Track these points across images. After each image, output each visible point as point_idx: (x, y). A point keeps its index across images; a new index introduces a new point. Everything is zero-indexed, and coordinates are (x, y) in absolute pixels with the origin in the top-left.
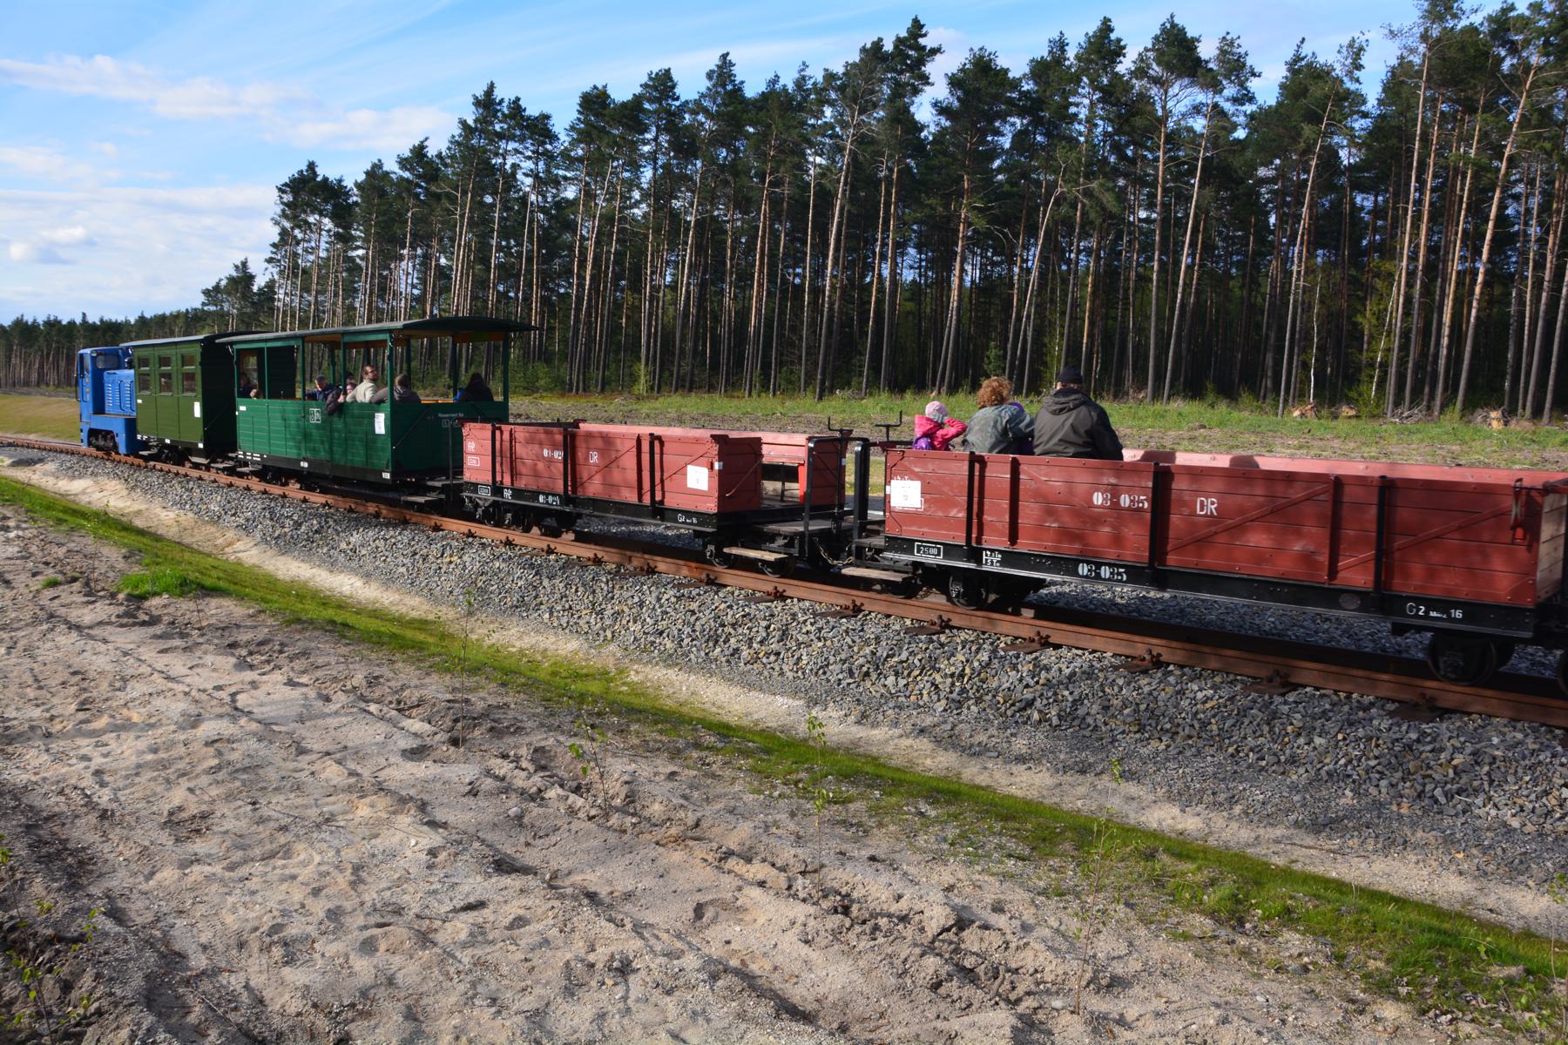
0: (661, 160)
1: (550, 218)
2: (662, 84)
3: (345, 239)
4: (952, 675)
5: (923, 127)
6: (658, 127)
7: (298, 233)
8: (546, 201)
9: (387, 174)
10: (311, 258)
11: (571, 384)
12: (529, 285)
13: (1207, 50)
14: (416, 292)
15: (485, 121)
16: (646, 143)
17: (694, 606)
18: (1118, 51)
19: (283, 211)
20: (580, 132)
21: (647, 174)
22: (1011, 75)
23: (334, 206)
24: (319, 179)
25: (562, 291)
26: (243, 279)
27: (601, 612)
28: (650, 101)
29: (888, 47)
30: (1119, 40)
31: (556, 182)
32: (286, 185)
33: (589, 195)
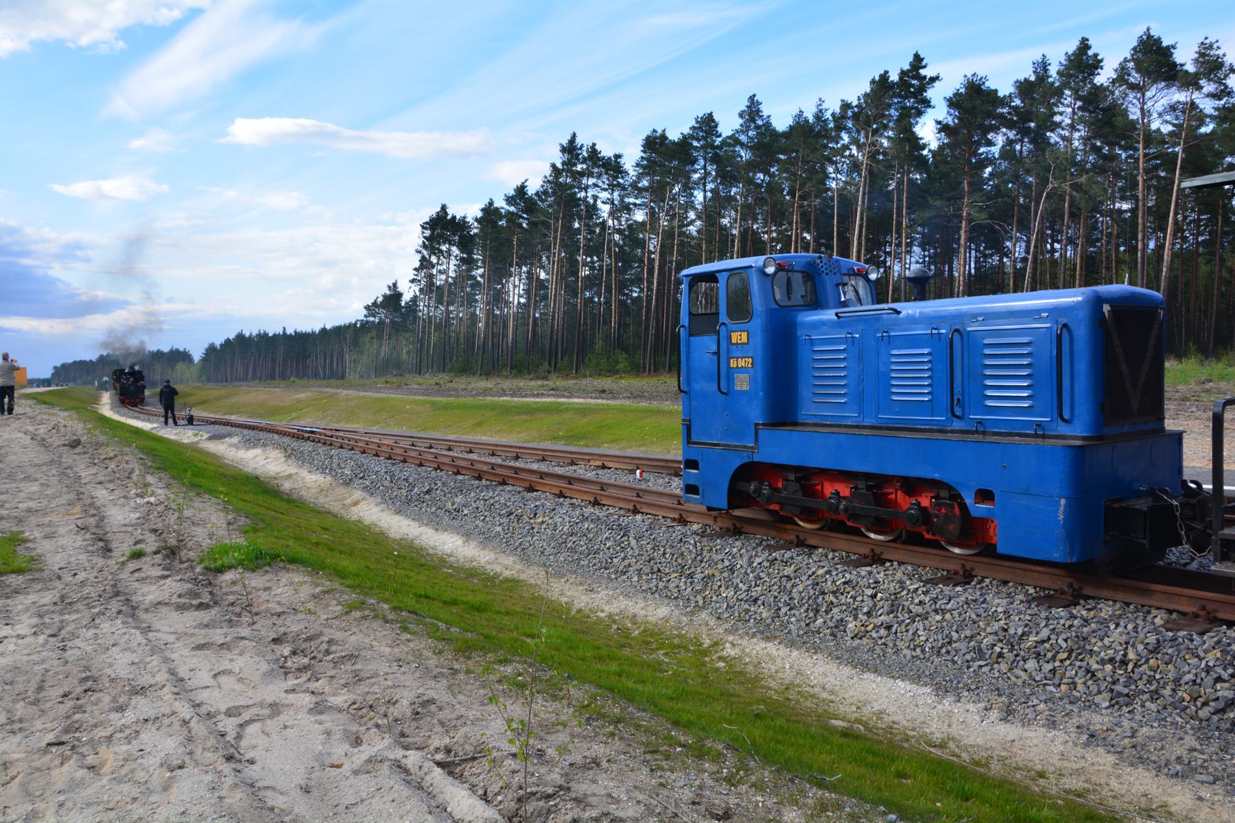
0: (710, 186)
1: (624, 237)
2: (707, 124)
3: (468, 262)
4: (1112, 660)
5: (924, 147)
6: (705, 159)
7: (434, 259)
8: (621, 225)
9: (497, 209)
10: (443, 277)
11: (645, 367)
12: (609, 290)
13: (1185, 57)
14: (522, 300)
15: (569, 164)
16: (696, 171)
17: (789, 571)
18: (1096, 64)
19: (424, 242)
20: (644, 167)
21: (699, 196)
22: (1001, 94)
23: (460, 237)
24: (449, 217)
25: (635, 295)
26: (393, 298)
27: (691, 576)
28: (698, 140)
29: (894, 77)
30: (1096, 55)
31: (627, 208)
32: (427, 223)
33: (652, 215)
